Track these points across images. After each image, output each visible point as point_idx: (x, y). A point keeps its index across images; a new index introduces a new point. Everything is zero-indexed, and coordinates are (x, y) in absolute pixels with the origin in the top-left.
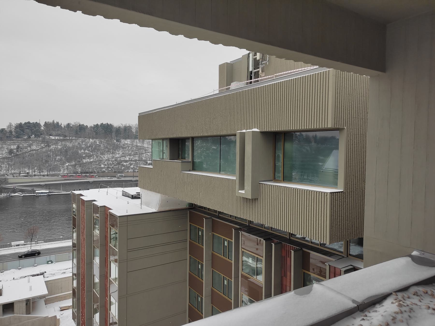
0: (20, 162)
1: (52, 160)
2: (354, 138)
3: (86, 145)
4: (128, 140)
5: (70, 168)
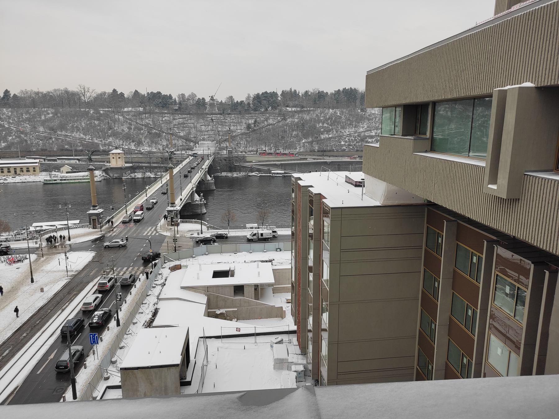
0: (257, 139)
3: (324, 117)
5: (307, 146)
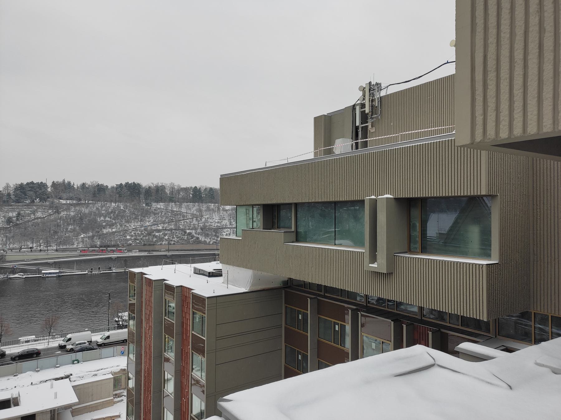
0: (21, 234)
1: (62, 231)
2: (506, 205)
4: (161, 204)
5: (86, 241)
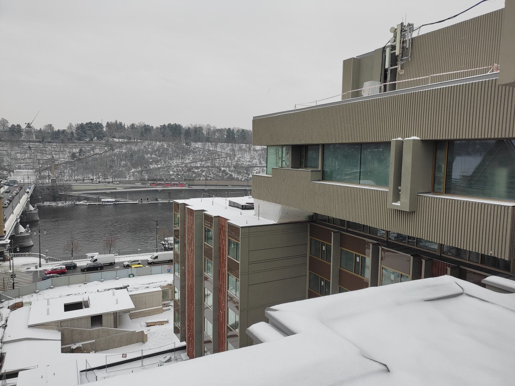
0: (83, 167)
4: (199, 143)
5: (136, 175)
